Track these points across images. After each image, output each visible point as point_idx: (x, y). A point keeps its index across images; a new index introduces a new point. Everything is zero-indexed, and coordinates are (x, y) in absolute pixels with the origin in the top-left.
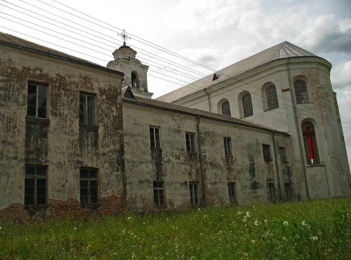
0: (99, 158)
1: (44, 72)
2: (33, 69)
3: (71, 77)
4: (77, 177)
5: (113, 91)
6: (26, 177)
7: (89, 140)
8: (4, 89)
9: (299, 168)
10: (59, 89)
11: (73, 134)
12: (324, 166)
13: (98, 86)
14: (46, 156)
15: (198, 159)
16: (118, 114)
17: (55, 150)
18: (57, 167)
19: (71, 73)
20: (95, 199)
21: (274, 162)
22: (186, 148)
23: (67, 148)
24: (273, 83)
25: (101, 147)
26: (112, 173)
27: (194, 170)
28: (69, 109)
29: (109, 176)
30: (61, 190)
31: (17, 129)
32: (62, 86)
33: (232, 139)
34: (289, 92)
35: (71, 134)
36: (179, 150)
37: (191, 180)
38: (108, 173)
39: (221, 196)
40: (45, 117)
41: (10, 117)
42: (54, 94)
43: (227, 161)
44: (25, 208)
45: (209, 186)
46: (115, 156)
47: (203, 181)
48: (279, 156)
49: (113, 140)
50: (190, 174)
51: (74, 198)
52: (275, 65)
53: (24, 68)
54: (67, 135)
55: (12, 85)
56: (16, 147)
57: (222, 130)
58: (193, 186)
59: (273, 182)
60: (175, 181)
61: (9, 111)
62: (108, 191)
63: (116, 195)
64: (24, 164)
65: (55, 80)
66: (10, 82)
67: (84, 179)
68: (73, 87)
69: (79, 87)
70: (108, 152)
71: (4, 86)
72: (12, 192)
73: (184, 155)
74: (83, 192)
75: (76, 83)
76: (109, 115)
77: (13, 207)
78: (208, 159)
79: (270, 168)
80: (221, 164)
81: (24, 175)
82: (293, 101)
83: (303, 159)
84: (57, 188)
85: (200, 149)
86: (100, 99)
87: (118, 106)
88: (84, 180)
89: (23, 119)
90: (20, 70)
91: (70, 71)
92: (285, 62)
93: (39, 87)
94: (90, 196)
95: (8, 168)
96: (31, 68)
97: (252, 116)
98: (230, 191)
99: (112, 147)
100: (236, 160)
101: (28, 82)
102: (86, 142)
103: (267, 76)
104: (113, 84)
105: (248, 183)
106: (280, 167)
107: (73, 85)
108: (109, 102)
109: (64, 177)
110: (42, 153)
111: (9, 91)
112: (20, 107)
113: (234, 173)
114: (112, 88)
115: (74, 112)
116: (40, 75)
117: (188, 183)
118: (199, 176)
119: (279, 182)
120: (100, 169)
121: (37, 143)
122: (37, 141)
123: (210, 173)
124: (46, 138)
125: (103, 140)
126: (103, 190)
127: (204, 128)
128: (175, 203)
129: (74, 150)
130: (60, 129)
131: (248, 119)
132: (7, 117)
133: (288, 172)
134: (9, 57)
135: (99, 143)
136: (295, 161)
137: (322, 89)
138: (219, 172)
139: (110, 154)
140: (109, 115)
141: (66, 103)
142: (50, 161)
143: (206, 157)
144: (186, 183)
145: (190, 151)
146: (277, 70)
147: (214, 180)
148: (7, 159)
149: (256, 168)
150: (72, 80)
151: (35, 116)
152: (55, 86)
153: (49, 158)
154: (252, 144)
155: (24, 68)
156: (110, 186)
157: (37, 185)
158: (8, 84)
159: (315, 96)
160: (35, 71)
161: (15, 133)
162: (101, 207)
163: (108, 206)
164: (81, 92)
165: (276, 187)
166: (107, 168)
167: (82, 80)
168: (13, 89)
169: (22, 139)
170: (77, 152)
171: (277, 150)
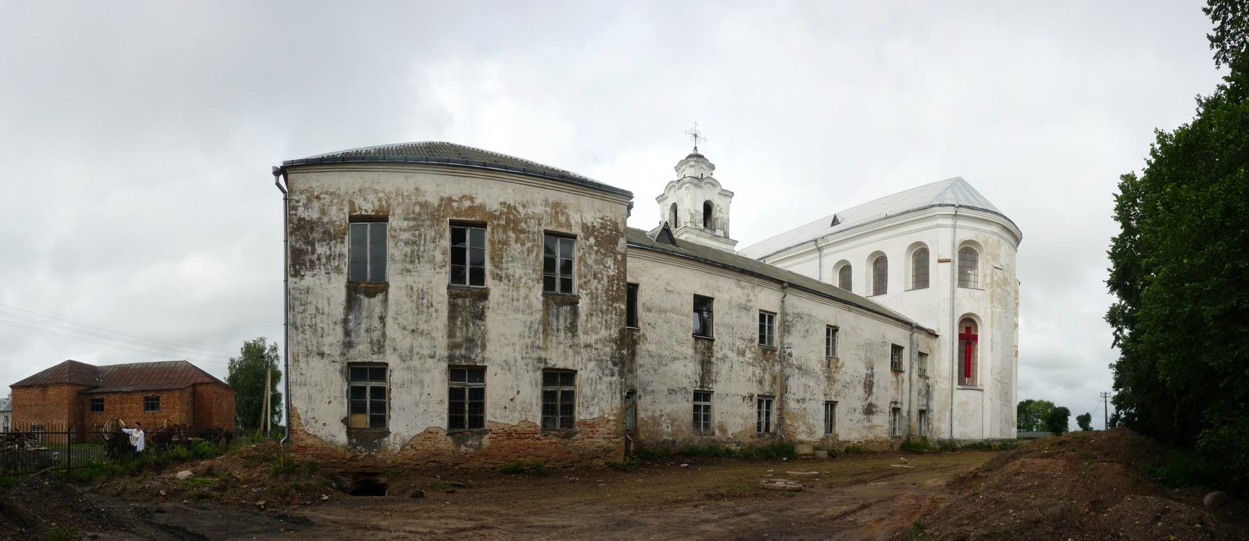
0: (578, 353)
1: (478, 202)
2: (457, 199)
3: (527, 205)
4: (537, 386)
5: (610, 229)
6: (450, 386)
7: (561, 320)
8: (410, 242)
9: (944, 389)
10: (505, 232)
11: (530, 312)
12: (982, 390)
13: (580, 221)
14: (482, 351)
15: (778, 359)
16: (618, 274)
17: (499, 341)
18: (502, 369)
19: (528, 197)
20: (569, 421)
21: (906, 376)
22: (758, 338)
23: (521, 335)
24: (926, 245)
25: (583, 333)
26: (600, 378)
27: (767, 377)
28: (525, 266)
29: (596, 383)
30: (507, 407)
31: (434, 309)
32: (512, 225)
33: (840, 330)
34: (949, 264)
35: (527, 311)
36: (744, 340)
37: (761, 393)
38: (594, 379)
39: (811, 421)
40: (484, 285)
41: (422, 290)
42: (497, 241)
43: (829, 365)
44: (448, 435)
45: (792, 405)
46: (608, 349)
47: (782, 395)
48: (916, 366)
49: (605, 320)
50: (760, 382)
51: (530, 420)
52: (934, 214)
53: (442, 199)
54: (521, 313)
55: (422, 234)
56: (433, 339)
57: (828, 313)
58: (764, 402)
59: (900, 407)
60: (734, 392)
61: (421, 279)
62: (591, 409)
63: (606, 416)
64: (447, 366)
65: (498, 213)
66: (419, 230)
67: (550, 389)
68: (531, 224)
69: (544, 223)
70: (596, 343)
71: (411, 237)
72: (428, 410)
73: (753, 349)
74: (548, 409)
75: (537, 217)
76: (600, 275)
77: (429, 432)
78: (794, 360)
79: (898, 384)
80: (817, 369)
81: (447, 383)
82: (953, 281)
83: (952, 377)
84: (501, 403)
85: (782, 343)
86: (583, 246)
87: (619, 257)
88: (549, 390)
89: (444, 291)
90: (436, 205)
91: (525, 194)
92: (951, 211)
93: (470, 232)
94: (560, 416)
95: (422, 371)
96: (453, 198)
97: (885, 295)
98: (826, 416)
99: (603, 333)
100: (843, 365)
101: (450, 224)
102: (555, 324)
103: (917, 231)
104: (610, 215)
105: (859, 405)
106: (915, 384)
107: (532, 221)
108: (602, 250)
109: (515, 385)
110: (476, 345)
111: (418, 245)
112: (438, 270)
113: (838, 386)
114: (609, 223)
115: (534, 270)
116: (470, 208)
117: (755, 399)
118: (777, 387)
119: (910, 408)
120: (579, 372)
121: (467, 330)
122: (467, 325)
123: (796, 384)
124: (483, 320)
125: (587, 321)
126: (583, 406)
127: (793, 306)
128: (729, 429)
129: (532, 339)
130: (509, 303)
131: (880, 300)
132: (417, 291)
133: (928, 393)
134: (415, 184)
135: (579, 325)
136: (940, 377)
137: (1001, 271)
138: (812, 383)
139: (599, 346)
140: (600, 275)
141: (518, 255)
142: (490, 359)
143: (791, 356)
144: (751, 397)
145: (764, 343)
146: (935, 222)
147: (801, 395)
148: (420, 358)
149: (875, 381)
150: (530, 212)
151: (465, 283)
152: (498, 225)
153: (487, 354)
154: (874, 342)
155: (442, 199)
156: (596, 400)
157: (469, 399)
158: (417, 232)
159: (988, 280)
160: (461, 202)
161: (431, 316)
162: (579, 436)
163: (591, 435)
164: (547, 233)
165: (905, 414)
166: (592, 371)
167: (548, 209)
168: (425, 240)
169: (443, 325)
170: (537, 343)
171: (916, 356)
